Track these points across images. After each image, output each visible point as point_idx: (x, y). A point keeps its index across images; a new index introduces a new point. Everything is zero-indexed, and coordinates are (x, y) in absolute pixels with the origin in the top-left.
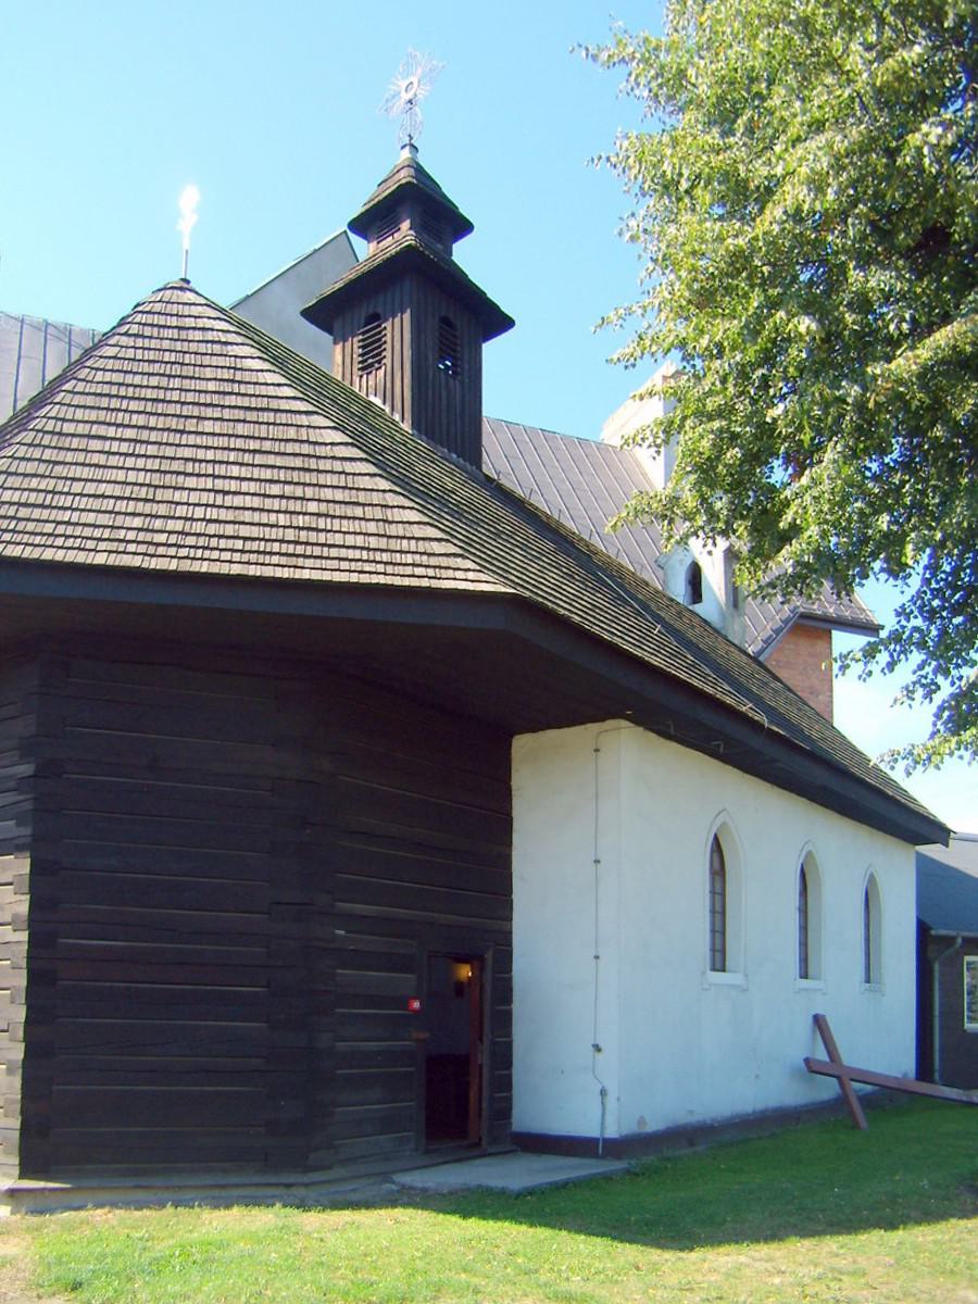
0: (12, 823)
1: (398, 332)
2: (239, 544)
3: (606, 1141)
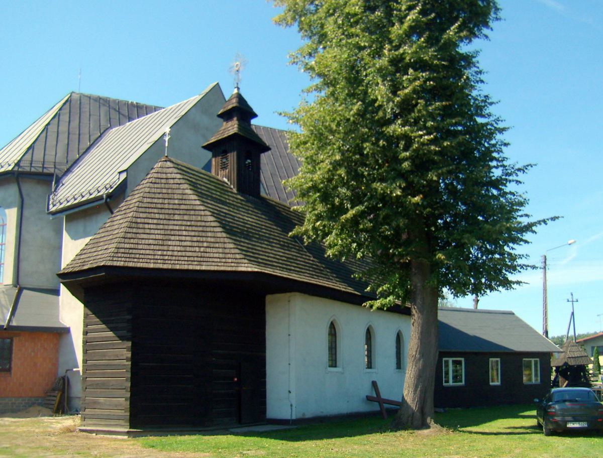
0: (125, 332)
1: (232, 157)
2: (186, 259)
3: (293, 420)
